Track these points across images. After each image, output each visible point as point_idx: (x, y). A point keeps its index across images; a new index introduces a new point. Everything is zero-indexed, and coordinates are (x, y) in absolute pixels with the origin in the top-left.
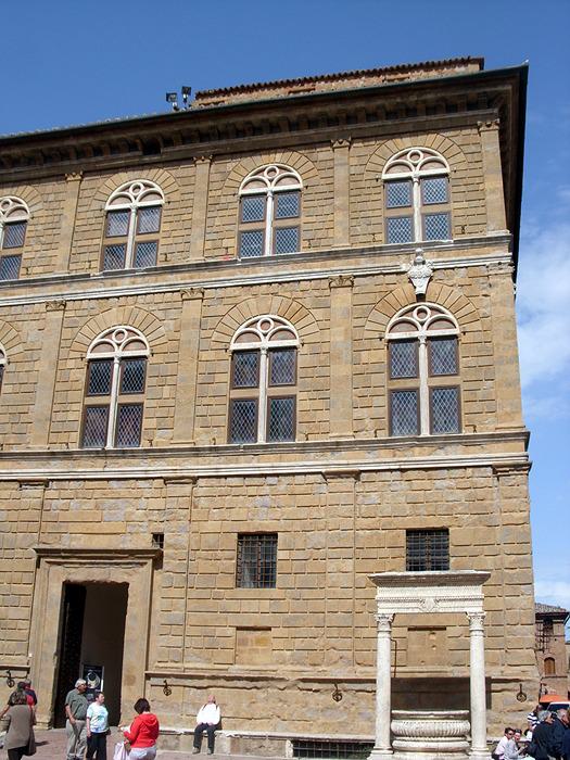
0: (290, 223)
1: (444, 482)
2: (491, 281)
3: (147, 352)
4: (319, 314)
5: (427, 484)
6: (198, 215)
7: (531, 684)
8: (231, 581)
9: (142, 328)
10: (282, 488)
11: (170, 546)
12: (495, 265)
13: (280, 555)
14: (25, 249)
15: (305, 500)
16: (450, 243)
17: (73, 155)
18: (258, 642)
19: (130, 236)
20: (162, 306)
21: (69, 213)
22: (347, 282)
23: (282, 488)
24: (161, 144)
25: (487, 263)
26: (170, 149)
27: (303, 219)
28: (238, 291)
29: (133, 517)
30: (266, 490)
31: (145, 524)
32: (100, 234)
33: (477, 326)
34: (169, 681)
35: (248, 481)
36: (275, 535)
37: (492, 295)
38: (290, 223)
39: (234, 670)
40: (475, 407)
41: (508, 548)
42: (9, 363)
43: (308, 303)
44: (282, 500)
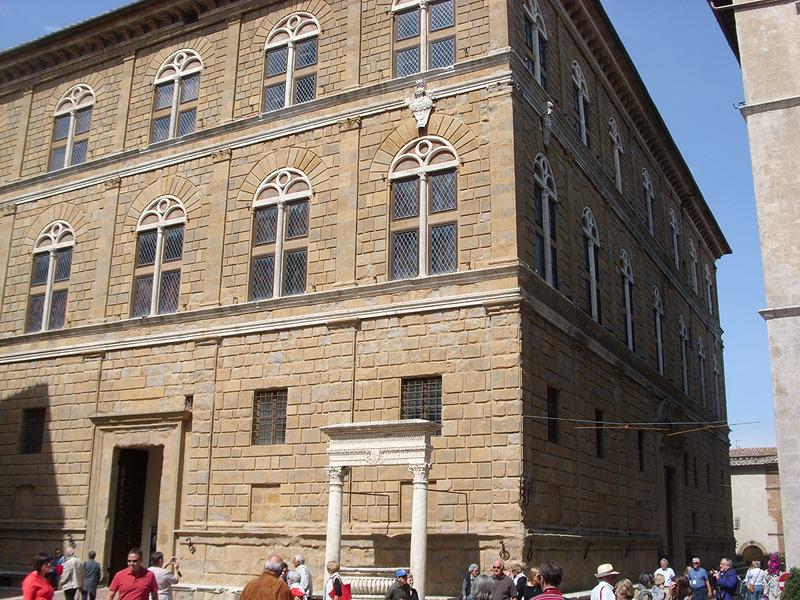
0: (308, 71)
1: (439, 325)
2: (491, 104)
3: (455, 163)
4: (328, 161)
5: (421, 329)
6: (228, 76)
7: (514, 541)
8: (247, 438)
9: (181, 196)
10: (292, 342)
11: (198, 407)
12: (494, 86)
13: (290, 410)
14: (458, 28)
15: (311, 353)
16: (450, 69)
17: (127, 36)
18: (271, 498)
19: (174, 108)
20: (197, 172)
21: (125, 92)
22: (357, 124)
23: (292, 342)
24: (198, 11)
25: (487, 86)
26: (205, 15)
27: (320, 65)
28: (260, 147)
29: (170, 381)
30: (279, 345)
31: (180, 387)
32: (149, 109)
33: (475, 155)
34: (193, 539)
35: (265, 338)
36: (285, 390)
37: (491, 119)
38: (308, 71)
39: (249, 528)
40: (472, 242)
41: (496, 394)
42: (463, 164)
43: (320, 151)
44: (292, 354)
